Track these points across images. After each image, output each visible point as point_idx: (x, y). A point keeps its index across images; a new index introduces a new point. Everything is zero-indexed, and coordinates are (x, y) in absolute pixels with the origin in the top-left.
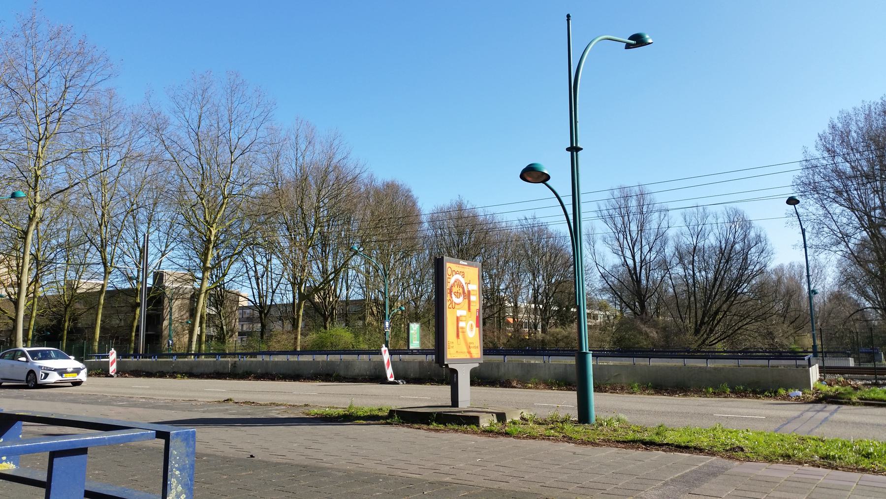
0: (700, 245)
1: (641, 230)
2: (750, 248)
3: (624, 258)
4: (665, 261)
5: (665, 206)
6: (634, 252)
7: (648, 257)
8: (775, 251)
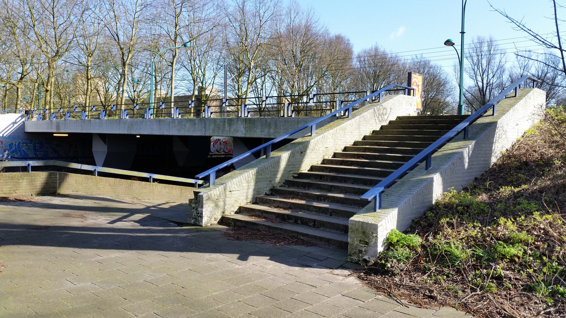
1: (489, 63)
3: (477, 81)
4: (502, 84)
6: (483, 77)
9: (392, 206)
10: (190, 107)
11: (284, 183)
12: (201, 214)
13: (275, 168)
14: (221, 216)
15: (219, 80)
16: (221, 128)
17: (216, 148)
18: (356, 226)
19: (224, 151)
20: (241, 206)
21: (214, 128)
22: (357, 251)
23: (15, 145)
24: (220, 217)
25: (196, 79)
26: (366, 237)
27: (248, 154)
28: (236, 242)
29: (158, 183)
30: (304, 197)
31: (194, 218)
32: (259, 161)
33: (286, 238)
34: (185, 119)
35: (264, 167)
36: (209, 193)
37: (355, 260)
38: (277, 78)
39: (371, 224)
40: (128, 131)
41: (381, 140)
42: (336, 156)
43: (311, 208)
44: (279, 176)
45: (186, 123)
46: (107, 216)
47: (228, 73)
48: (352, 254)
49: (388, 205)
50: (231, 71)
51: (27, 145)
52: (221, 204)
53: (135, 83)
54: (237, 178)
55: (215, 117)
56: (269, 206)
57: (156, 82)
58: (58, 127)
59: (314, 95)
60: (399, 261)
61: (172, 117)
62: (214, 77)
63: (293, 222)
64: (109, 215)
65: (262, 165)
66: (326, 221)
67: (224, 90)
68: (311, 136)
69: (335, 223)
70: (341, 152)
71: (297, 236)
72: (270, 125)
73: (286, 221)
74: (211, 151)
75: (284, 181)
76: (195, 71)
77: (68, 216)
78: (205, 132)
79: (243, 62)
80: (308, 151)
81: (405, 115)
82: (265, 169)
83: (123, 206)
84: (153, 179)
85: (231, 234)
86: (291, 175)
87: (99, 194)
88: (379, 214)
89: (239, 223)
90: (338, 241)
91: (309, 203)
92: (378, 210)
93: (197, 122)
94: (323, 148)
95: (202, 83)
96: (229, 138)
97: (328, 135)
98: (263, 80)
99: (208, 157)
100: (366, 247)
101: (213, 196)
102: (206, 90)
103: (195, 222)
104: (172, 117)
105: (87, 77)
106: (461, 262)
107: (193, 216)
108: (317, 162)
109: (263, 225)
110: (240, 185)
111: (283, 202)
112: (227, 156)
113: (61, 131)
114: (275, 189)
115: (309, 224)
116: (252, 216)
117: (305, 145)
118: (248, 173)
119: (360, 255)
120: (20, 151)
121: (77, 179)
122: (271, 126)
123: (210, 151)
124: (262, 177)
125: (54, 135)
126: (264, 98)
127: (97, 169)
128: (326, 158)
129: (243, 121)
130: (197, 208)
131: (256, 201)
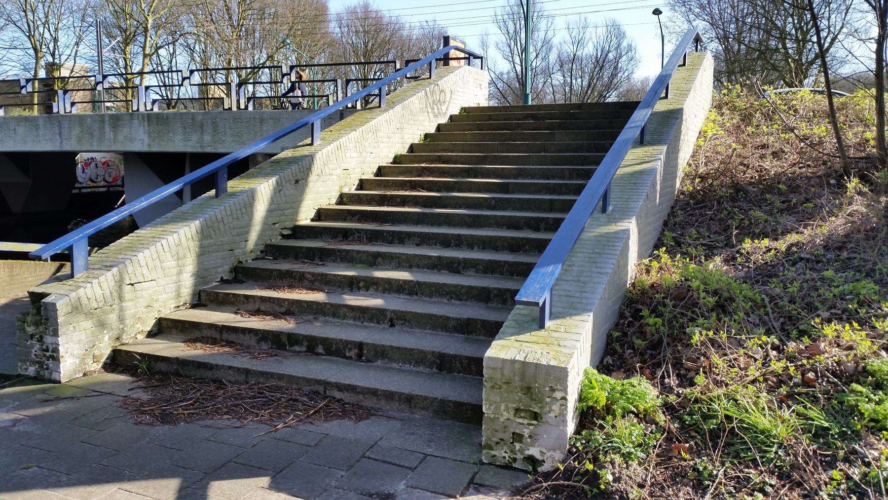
0: (579, 53)
2: (620, 57)
5: (552, 13)
7: (534, 64)
8: (642, 60)
9: (576, 309)
11: (262, 252)
12: (53, 351)
13: (241, 219)
14: (110, 349)
15: (87, 49)
17: (89, 175)
18: (506, 372)
19: (104, 180)
20: (162, 316)
21: (80, 136)
22: (508, 437)
24: (107, 352)
25: (39, 47)
26: (532, 399)
27: (173, 188)
28: (161, 430)
30: (317, 283)
31: (34, 363)
32: (201, 204)
33: (297, 400)
34: (13, 118)
35: (214, 218)
36: (73, 295)
37: (500, 459)
38: (197, 48)
39: (549, 366)
41: (445, 151)
42: (364, 186)
43: (342, 311)
44: (253, 236)
45: (18, 125)
47: (103, 37)
48: (493, 444)
49: (565, 308)
50: (110, 36)
52: (113, 317)
54: (146, 251)
55: (80, 112)
56: (235, 309)
59: (292, 68)
60: (627, 457)
62: (77, 44)
63: (304, 349)
66: (388, 344)
67: (97, 68)
68: (311, 144)
69: (412, 350)
70: (372, 177)
71: (325, 392)
72: (202, 126)
73: (286, 350)
74: (78, 181)
75: (262, 248)
76: (36, 32)
78: (62, 142)
79: (131, 16)
80: (312, 178)
81: (472, 105)
82: (216, 224)
85: (142, 405)
86: (276, 233)
88: (555, 334)
89: (163, 367)
90: (436, 399)
91: (335, 300)
92: (548, 324)
93: (41, 122)
94: (339, 171)
95: (53, 55)
97: (348, 142)
99: (74, 191)
100: (532, 425)
101: (84, 301)
102: (62, 69)
103: (38, 372)
106: (780, 446)
107: (33, 356)
108: (329, 201)
109: (230, 368)
110: (155, 267)
112: (111, 189)
115: (347, 354)
116: (195, 341)
117: (304, 166)
118: (175, 235)
119: (518, 446)
122: (205, 128)
124: (212, 241)
128: (346, 190)
130: (41, 337)
131: (200, 300)
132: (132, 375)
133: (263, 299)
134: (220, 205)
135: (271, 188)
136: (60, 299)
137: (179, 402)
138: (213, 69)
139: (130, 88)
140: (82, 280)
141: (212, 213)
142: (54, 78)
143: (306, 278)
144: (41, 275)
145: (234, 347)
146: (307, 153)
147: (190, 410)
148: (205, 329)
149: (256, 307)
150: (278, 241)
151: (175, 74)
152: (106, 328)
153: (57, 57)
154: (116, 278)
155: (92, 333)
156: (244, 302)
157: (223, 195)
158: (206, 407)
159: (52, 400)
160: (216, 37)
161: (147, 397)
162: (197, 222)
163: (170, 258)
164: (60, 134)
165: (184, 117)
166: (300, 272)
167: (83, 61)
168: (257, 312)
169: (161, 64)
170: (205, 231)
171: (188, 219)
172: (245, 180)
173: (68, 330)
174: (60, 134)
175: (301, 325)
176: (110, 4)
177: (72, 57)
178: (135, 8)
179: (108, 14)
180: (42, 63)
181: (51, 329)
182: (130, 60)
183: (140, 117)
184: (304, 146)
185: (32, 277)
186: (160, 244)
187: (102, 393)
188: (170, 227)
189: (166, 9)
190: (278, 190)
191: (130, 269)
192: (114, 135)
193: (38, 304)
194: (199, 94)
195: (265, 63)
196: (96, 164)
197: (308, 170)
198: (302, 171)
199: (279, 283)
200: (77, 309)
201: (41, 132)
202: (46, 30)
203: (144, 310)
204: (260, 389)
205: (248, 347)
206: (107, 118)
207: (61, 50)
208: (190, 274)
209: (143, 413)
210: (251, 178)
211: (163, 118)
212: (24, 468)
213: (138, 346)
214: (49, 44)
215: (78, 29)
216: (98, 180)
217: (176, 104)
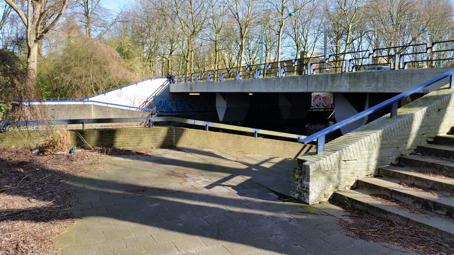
10: (294, 65)
11: (415, 150)
12: (306, 189)
13: (404, 130)
14: (333, 192)
15: (320, 44)
16: (324, 84)
17: (316, 103)
19: (323, 105)
20: (359, 179)
23: (163, 102)
24: (331, 193)
25: (299, 44)
28: (360, 242)
29: (262, 138)
31: (298, 192)
33: (441, 245)
34: (288, 77)
35: (389, 129)
36: (317, 162)
38: (373, 38)
40: (241, 89)
44: (411, 141)
46: (207, 177)
50: (331, 36)
51: (171, 102)
52: (335, 176)
53: (251, 52)
54: (353, 144)
56: (399, 181)
57: (267, 50)
58: (191, 88)
61: (277, 76)
62: (315, 42)
64: (210, 175)
65: (388, 126)
72: (378, 79)
73: (431, 211)
75: (415, 148)
76: (298, 38)
77: (172, 174)
78: (308, 88)
82: (390, 133)
83: (226, 164)
84: (258, 134)
85: (349, 225)
86: (424, 140)
87: (210, 147)
89: (360, 207)
93: (300, 79)
95: (304, 48)
96: (329, 94)
98: (360, 41)
101: (322, 166)
103: (299, 197)
104: (277, 76)
105: (216, 49)
107: (297, 189)
109: (397, 215)
110: (357, 153)
111: (421, 179)
112: (326, 110)
113: (193, 91)
114: (404, 159)
118: (368, 137)
120: (166, 106)
121: (191, 133)
122: (379, 79)
123: (311, 106)
125: (190, 94)
126: (371, 51)
127: (208, 124)
129: (347, 76)
130: (302, 181)
131: (379, 174)
132: (343, 208)
133: (416, 178)
134: (393, 122)
135: (423, 113)
136: (312, 164)
137: (369, 228)
138: (381, 49)
139: (338, 61)
140: (322, 156)
141: (388, 126)
142: (304, 58)
143: (444, 169)
144: (296, 149)
145: (399, 203)
146: (446, 93)
147: (375, 234)
148: (383, 190)
149: (412, 182)
150: (425, 144)
151: (360, 53)
152: (331, 181)
153: (306, 48)
154: (338, 157)
155: (325, 183)
156: (404, 178)
157: (394, 117)
158: (384, 235)
159: (305, 213)
160: (384, 31)
161: (351, 222)
162: (380, 131)
163: (365, 149)
164: (307, 84)
165: (368, 74)
166: (441, 165)
167: (317, 49)
168: (412, 185)
169: (354, 48)
170: (384, 136)
171: (375, 129)
172: (407, 109)
173: (314, 179)
174: (307, 84)
175: (442, 198)
176: (332, 21)
177: (312, 48)
178: (343, 21)
179: (330, 26)
180: (299, 52)
181: (306, 178)
182: (339, 47)
183: (346, 75)
184: (444, 89)
185: (293, 149)
186: (360, 141)
187: (329, 215)
188: (365, 133)
189: (359, 20)
190: (427, 115)
191: (345, 153)
192: (332, 84)
193: (300, 165)
194: (372, 62)
195: (410, 43)
196: (320, 98)
197: (447, 103)
198: (443, 104)
199: (426, 170)
200: (319, 170)
201: (299, 83)
202: (302, 36)
203: (350, 175)
204: (416, 231)
205: (408, 205)
206: (329, 76)
207: (308, 45)
208: (375, 159)
209: (350, 230)
210: (411, 107)
211: (358, 75)
212: (295, 245)
213: (346, 193)
214: (303, 43)
215: (316, 34)
216: (320, 105)
217: (360, 67)
